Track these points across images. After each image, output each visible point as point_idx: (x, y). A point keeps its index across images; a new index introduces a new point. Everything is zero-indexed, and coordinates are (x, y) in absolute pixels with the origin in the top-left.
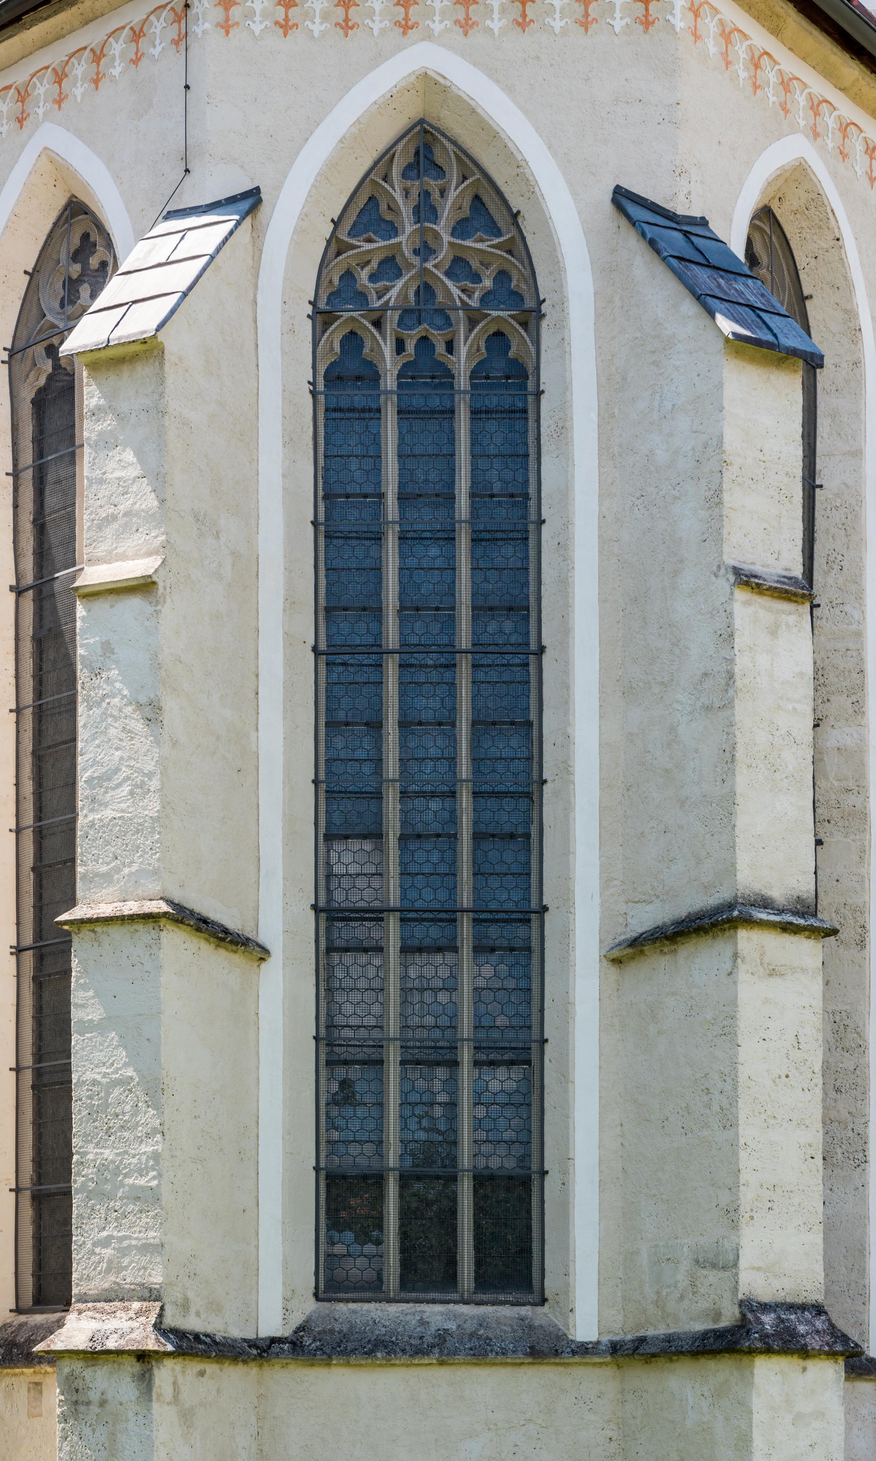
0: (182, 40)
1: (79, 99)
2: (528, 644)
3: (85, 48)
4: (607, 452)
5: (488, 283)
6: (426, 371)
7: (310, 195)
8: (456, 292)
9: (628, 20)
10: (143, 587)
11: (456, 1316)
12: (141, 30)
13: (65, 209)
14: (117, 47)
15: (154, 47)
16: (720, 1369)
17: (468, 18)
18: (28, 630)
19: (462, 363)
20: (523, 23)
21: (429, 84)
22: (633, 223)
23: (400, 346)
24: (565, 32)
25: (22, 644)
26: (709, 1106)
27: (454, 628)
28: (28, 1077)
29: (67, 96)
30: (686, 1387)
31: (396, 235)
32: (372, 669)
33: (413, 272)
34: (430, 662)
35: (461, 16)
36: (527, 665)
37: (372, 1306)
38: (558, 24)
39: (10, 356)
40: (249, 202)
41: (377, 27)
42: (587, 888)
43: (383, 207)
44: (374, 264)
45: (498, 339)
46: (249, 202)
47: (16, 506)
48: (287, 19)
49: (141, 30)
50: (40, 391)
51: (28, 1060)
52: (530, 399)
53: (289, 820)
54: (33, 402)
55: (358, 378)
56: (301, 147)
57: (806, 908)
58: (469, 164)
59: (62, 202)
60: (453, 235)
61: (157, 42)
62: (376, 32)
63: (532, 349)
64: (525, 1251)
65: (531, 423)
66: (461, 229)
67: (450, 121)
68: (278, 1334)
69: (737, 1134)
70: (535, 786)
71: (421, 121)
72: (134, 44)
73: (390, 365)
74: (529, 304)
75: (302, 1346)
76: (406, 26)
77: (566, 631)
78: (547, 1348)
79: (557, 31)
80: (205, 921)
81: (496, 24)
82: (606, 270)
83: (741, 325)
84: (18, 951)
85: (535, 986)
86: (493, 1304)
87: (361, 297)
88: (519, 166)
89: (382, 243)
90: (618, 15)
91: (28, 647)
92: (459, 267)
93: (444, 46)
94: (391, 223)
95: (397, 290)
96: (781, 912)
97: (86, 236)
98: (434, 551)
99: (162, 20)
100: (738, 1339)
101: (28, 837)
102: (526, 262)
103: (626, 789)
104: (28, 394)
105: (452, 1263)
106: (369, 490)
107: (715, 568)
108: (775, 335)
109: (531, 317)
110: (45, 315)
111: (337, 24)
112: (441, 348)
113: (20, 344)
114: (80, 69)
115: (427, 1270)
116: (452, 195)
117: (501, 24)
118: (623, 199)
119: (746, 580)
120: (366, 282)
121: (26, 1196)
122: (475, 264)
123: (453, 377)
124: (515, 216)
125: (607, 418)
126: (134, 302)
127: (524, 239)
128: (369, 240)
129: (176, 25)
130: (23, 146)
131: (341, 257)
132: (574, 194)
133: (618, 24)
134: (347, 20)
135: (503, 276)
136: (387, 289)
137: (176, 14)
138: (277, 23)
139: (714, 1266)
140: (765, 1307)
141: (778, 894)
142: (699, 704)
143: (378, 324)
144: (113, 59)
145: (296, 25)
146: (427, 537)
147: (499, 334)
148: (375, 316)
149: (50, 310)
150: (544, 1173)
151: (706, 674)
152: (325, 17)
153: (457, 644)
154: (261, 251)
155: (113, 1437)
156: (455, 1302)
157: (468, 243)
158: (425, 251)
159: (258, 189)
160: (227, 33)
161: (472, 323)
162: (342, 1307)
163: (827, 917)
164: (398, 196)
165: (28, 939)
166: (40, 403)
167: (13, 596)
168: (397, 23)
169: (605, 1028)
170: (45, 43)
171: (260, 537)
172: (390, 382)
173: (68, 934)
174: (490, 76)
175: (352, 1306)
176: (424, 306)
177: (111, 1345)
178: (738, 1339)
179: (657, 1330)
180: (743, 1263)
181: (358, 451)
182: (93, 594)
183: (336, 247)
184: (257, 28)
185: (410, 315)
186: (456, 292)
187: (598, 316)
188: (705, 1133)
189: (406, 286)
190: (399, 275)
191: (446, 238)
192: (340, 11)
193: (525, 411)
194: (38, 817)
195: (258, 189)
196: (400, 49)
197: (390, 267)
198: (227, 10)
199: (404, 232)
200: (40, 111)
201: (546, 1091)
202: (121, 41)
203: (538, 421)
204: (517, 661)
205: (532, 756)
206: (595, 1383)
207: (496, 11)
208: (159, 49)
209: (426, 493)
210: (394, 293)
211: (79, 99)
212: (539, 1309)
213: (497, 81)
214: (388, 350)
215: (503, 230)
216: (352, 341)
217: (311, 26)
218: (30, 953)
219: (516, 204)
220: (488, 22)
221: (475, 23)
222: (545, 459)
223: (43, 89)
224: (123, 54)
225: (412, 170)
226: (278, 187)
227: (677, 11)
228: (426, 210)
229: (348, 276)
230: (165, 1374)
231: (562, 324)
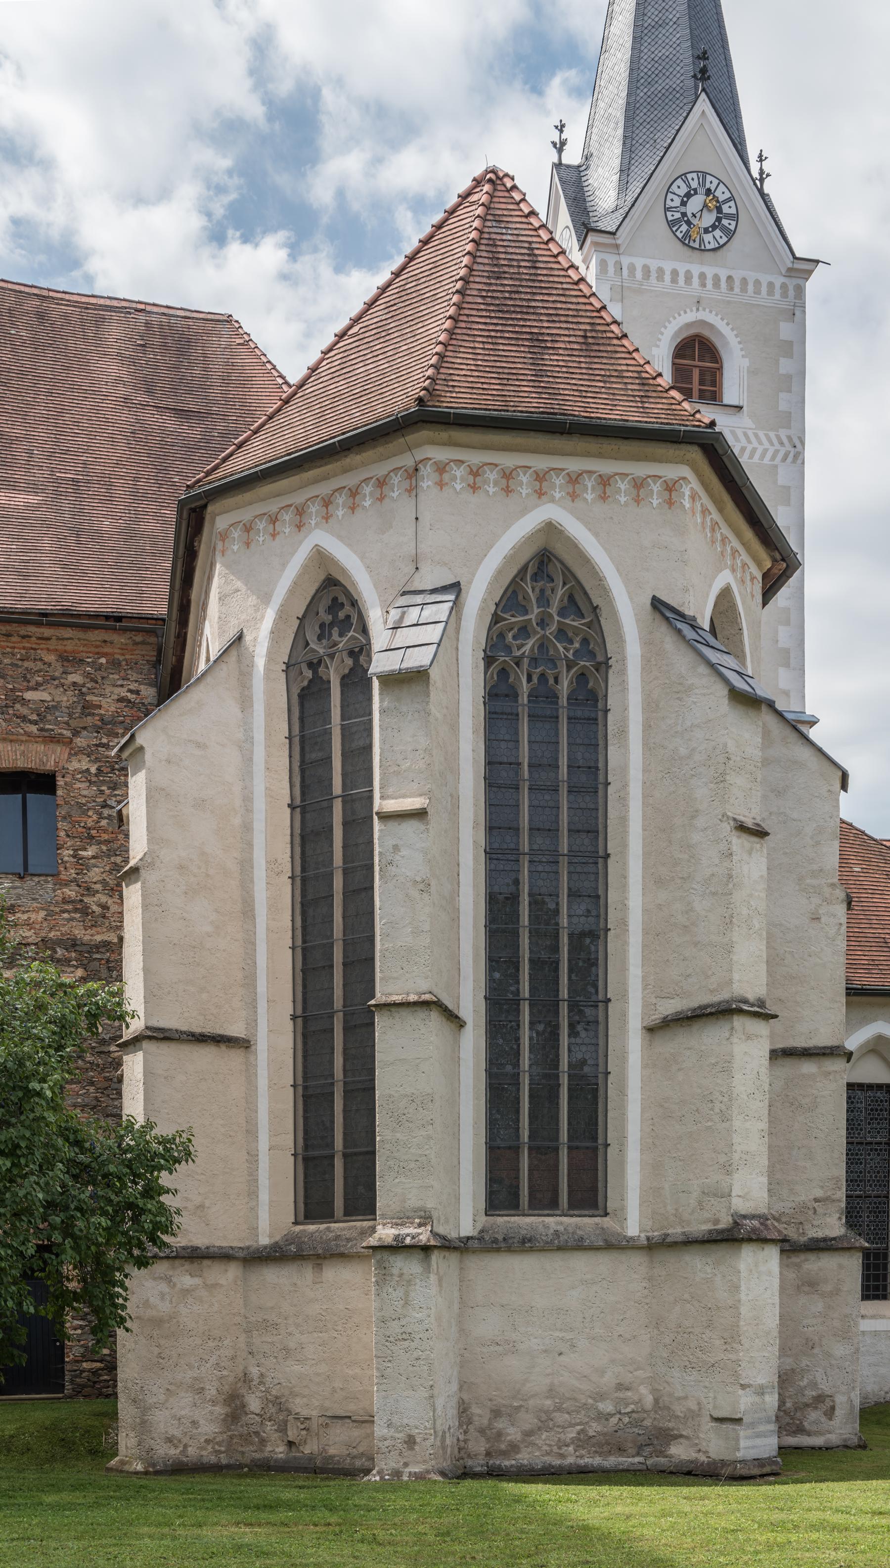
0: (413, 490)
1: (340, 518)
2: (598, 852)
3: (344, 487)
4: (647, 746)
5: (577, 645)
6: (544, 694)
7: (487, 589)
8: (561, 649)
9: (660, 500)
10: (420, 814)
11: (561, 1223)
12: (384, 481)
13: (324, 581)
14: (367, 489)
15: (394, 492)
16: (721, 1252)
17: (574, 492)
18: (298, 831)
19: (564, 687)
20: (604, 497)
21: (550, 529)
22: (667, 619)
23: (529, 679)
24: (626, 504)
25: (294, 838)
26: (712, 1109)
27: (558, 841)
28: (300, 1090)
29: (332, 515)
30: (698, 1265)
31: (526, 612)
32: (513, 863)
33: (539, 636)
34: (544, 860)
35: (571, 490)
36: (597, 863)
37: (516, 1218)
38: (623, 499)
39: (287, 667)
40: (455, 587)
41: (524, 492)
42: (634, 988)
43: (520, 598)
44: (516, 630)
45: (582, 677)
46: (455, 587)
47: (290, 757)
48: (475, 483)
49: (384, 481)
50: (303, 689)
51: (300, 1081)
52: (600, 714)
53: (475, 948)
54: (299, 695)
55: (507, 696)
56: (483, 559)
57: (761, 1003)
58: (569, 575)
59: (323, 577)
60: (558, 615)
61: (396, 489)
62: (524, 495)
63: (603, 685)
64: (594, 1190)
65: (600, 727)
66: (562, 612)
67: (560, 550)
68: (470, 1235)
69: (731, 1125)
70: (602, 932)
71: (545, 549)
72: (379, 489)
73: (525, 687)
74: (600, 658)
75: (486, 1244)
76: (540, 494)
77: (624, 845)
79: (623, 503)
81: (589, 496)
82: (647, 643)
84: (294, 1018)
85: (601, 1042)
86: (580, 1216)
87: (508, 649)
88: (600, 580)
89: (521, 618)
90: (655, 497)
91: (298, 840)
92: (562, 633)
93: (561, 506)
94: (524, 607)
95: (529, 645)
96: (752, 1005)
97: (335, 599)
98: (547, 797)
99: (399, 476)
100: (731, 1237)
101: (299, 951)
102: (600, 635)
103: (654, 934)
104: (296, 691)
105: (516, 1195)
106: (512, 760)
107: (720, 817)
108: (753, 689)
109: (603, 666)
110: (307, 644)
111: (502, 489)
112: (551, 681)
113: (293, 662)
114: (341, 500)
115: (544, 1201)
116: (560, 593)
117: (592, 497)
118: (657, 604)
119: (760, 833)
120: (511, 640)
121: (300, 1158)
122: (570, 634)
123: (558, 698)
124: (595, 608)
125: (647, 727)
126: (408, 647)
127: (599, 621)
128: (513, 616)
129: (408, 481)
130: (301, 542)
131: (499, 625)
132: (631, 599)
133: (655, 502)
134: (508, 487)
135: (585, 641)
136: (523, 645)
137: (408, 474)
138: (469, 485)
139: (715, 1195)
140: (745, 1217)
141: (751, 997)
142: (708, 891)
143: (517, 664)
144: (365, 495)
145: (480, 488)
147: (583, 674)
148: (516, 660)
149: (313, 641)
150: (607, 1145)
151: (713, 875)
152: (496, 484)
153: (560, 849)
154: (460, 619)
155: (407, 1294)
156: (560, 1216)
157: (567, 621)
159: (459, 582)
160: (441, 489)
161: (569, 668)
162: (500, 1220)
163: (771, 1009)
164: (530, 591)
165: (299, 1012)
166: (303, 696)
167: (288, 811)
168: (536, 491)
169: (644, 1066)
170: (316, 481)
171: (460, 785)
172: (524, 699)
173: (373, 1013)
174: (586, 527)
175: (506, 1218)
177: (408, 1241)
178: (731, 1237)
179: (676, 1231)
180: (734, 1194)
181: (507, 737)
182: (385, 817)
183: (496, 619)
184: (458, 487)
186: (561, 649)
187: (643, 669)
188: (710, 1124)
189: (533, 645)
190: (528, 637)
191: (556, 618)
192: (504, 481)
193: (596, 719)
194: (304, 942)
195: (459, 582)
196: (537, 506)
197: (524, 631)
198: (441, 474)
199: (533, 613)
200: (313, 522)
201: (609, 1100)
202: (370, 486)
203: (606, 725)
204: (591, 861)
206: (637, 1260)
207: (590, 488)
208: (396, 493)
209: (544, 764)
210: (527, 648)
211: (340, 518)
212: (605, 1219)
213: (590, 530)
214: (524, 680)
215: (586, 615)
216: (503, 673)
217: (488, 489)
218: (300, 1019)
219: (596, 601)
220: (585, 495)
221: (578, 495)
222: (610, 748)
223: (314, 509)
224: (371, 494)
225: (535, 577)
226: (470, 582)
227: (686, 497)
228: (544, 600)
229: (501, 636)
230: (435, 1257)
231: (623, 672)
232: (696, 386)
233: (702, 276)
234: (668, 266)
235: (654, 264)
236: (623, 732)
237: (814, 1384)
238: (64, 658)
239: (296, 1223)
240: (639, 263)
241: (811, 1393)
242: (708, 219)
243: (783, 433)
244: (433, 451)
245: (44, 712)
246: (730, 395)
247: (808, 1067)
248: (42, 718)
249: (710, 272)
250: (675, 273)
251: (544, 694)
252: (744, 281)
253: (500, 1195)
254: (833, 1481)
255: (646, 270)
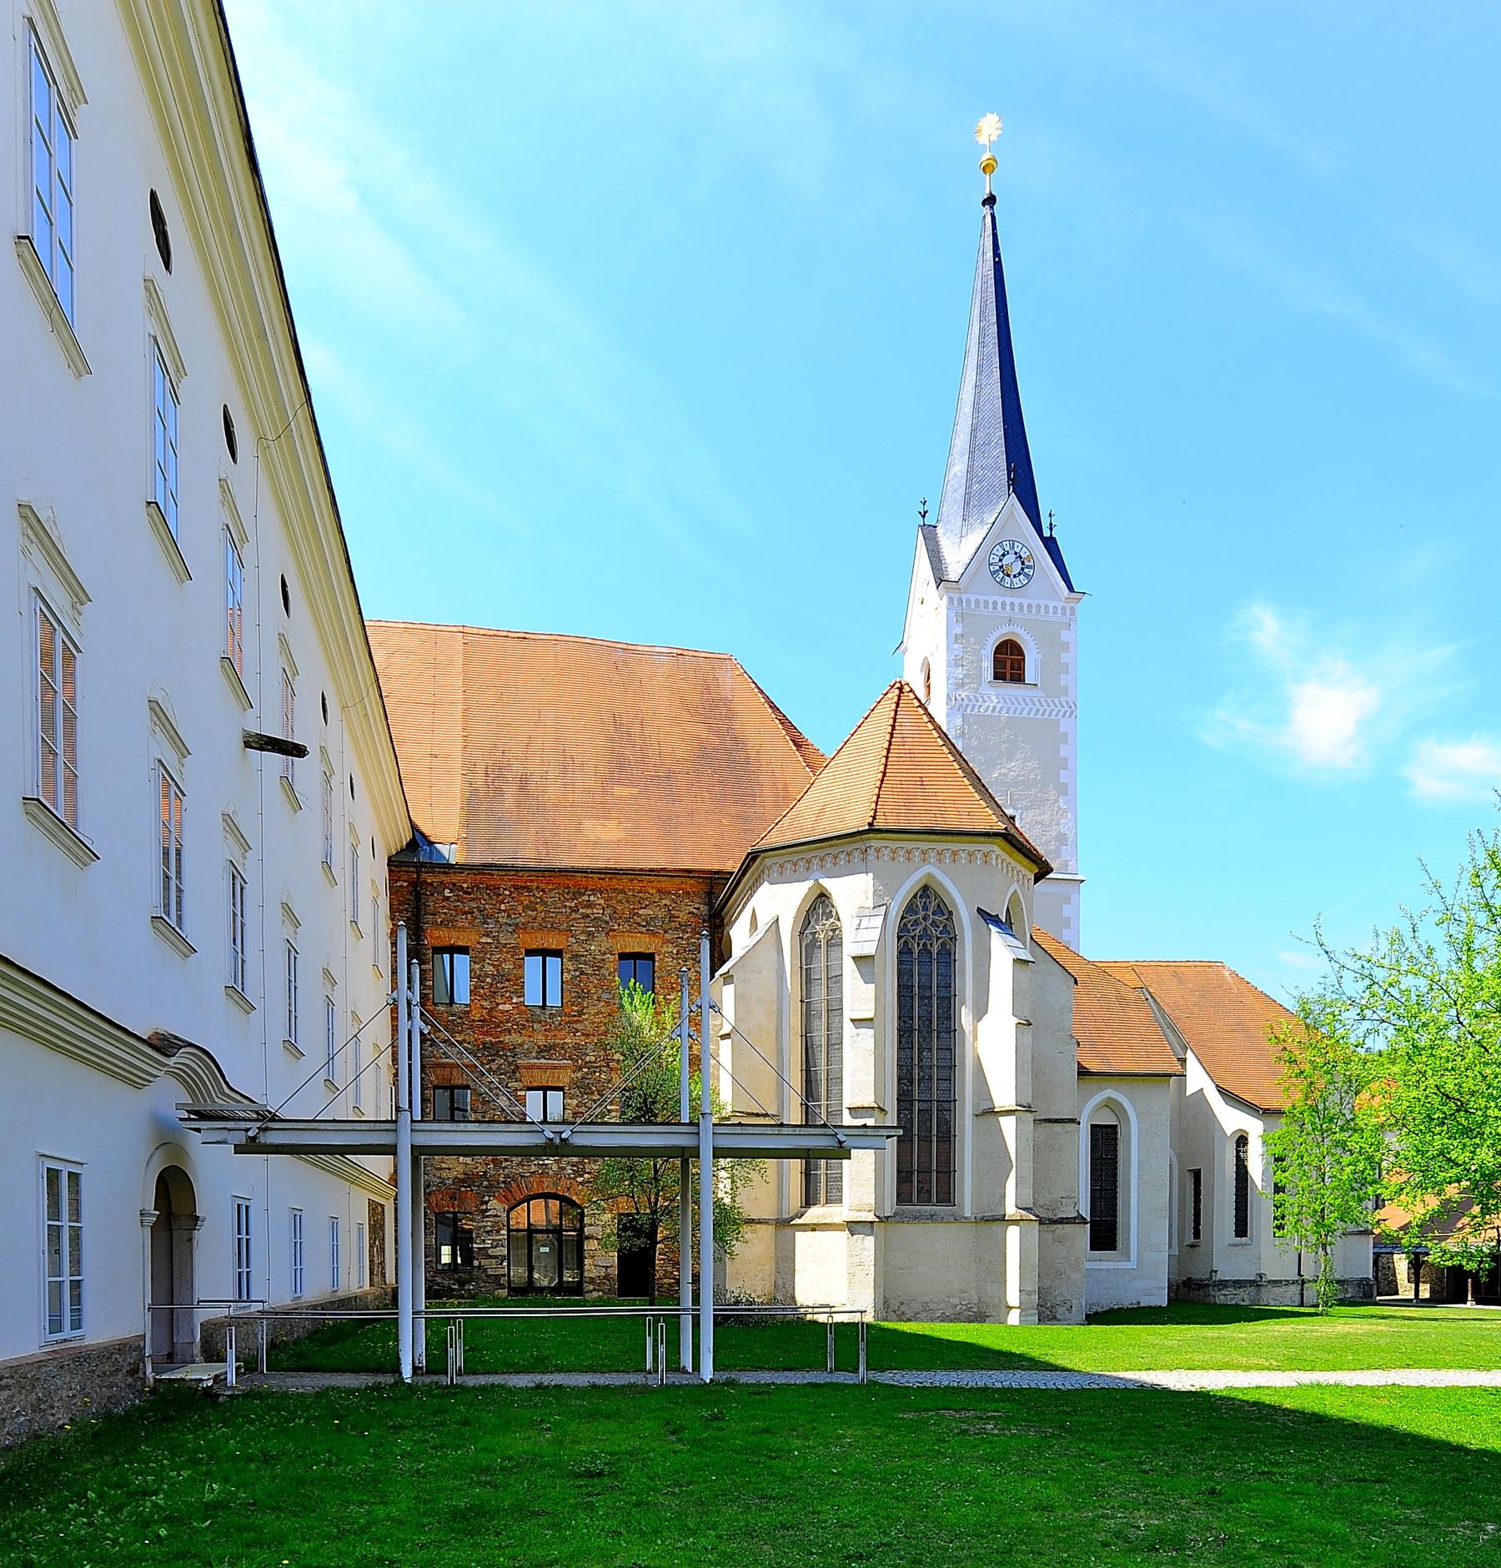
4: (1472, 1390)
6: (925, 951)
45: (943, 945)
58: (937, 896)
67: (933, 885)
78: (958, 1219)
80: (79, 1262)
82: (975, 929)
83: (1166, 1392)
92: (934, 924)
115: (925, 1198)
125: (975, 969)
146: (926, 999)
158: (925, 919)
176: (925, 934)
185: (921, 938)
197: (916, 923)
205: (952, 1059)
206: (970, 1228)
228: (925, 908)
232: (1008, 671)
233: (1012, 604)
234: (991, 600)
235: (982, 599)
236: (963, 972)
237: (1061, 1295)
238: (659, 891)
239: (415, 873)
240: (973, 598)
241: (1059, 1299)
242: (1017, 567)
243: (1063, 699)
244: (875, 842)
245: (649, 921)
246: (1029, 677)
247: (1057, 1127)
248: (648, 924)
249: (1017, 601)
250: (995, 603)
251: (925, 951)
252: (1039, 606)
253: (902, 1197)
254: (1459, 1449)
255: (977, 602)
